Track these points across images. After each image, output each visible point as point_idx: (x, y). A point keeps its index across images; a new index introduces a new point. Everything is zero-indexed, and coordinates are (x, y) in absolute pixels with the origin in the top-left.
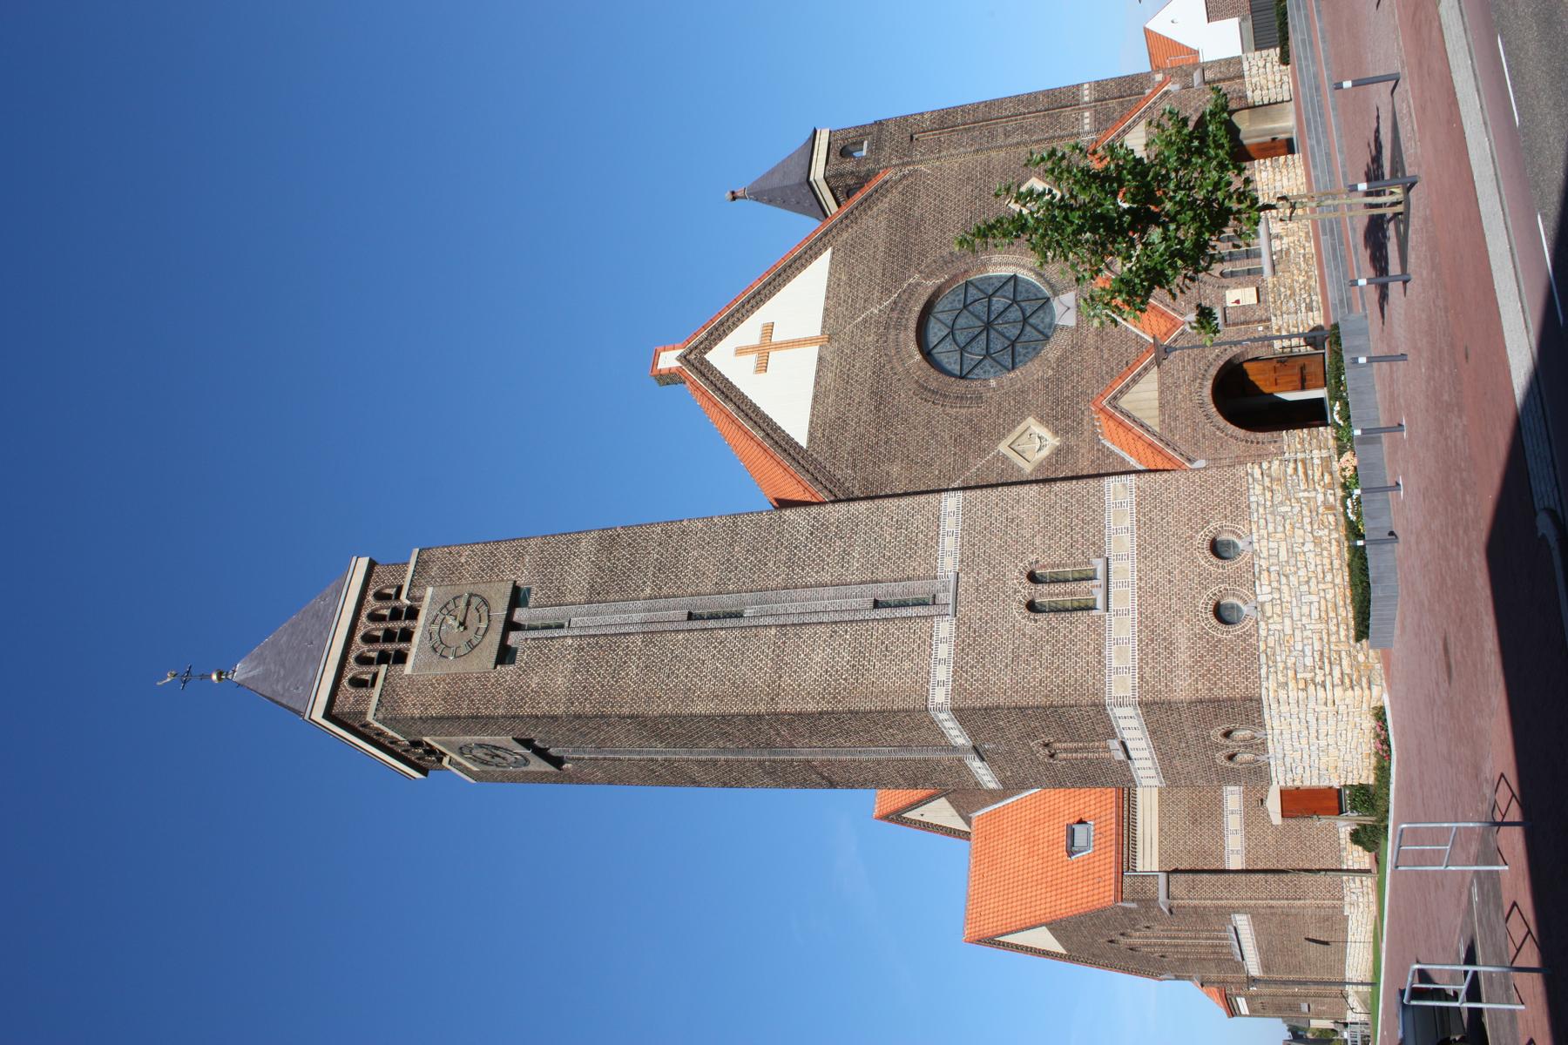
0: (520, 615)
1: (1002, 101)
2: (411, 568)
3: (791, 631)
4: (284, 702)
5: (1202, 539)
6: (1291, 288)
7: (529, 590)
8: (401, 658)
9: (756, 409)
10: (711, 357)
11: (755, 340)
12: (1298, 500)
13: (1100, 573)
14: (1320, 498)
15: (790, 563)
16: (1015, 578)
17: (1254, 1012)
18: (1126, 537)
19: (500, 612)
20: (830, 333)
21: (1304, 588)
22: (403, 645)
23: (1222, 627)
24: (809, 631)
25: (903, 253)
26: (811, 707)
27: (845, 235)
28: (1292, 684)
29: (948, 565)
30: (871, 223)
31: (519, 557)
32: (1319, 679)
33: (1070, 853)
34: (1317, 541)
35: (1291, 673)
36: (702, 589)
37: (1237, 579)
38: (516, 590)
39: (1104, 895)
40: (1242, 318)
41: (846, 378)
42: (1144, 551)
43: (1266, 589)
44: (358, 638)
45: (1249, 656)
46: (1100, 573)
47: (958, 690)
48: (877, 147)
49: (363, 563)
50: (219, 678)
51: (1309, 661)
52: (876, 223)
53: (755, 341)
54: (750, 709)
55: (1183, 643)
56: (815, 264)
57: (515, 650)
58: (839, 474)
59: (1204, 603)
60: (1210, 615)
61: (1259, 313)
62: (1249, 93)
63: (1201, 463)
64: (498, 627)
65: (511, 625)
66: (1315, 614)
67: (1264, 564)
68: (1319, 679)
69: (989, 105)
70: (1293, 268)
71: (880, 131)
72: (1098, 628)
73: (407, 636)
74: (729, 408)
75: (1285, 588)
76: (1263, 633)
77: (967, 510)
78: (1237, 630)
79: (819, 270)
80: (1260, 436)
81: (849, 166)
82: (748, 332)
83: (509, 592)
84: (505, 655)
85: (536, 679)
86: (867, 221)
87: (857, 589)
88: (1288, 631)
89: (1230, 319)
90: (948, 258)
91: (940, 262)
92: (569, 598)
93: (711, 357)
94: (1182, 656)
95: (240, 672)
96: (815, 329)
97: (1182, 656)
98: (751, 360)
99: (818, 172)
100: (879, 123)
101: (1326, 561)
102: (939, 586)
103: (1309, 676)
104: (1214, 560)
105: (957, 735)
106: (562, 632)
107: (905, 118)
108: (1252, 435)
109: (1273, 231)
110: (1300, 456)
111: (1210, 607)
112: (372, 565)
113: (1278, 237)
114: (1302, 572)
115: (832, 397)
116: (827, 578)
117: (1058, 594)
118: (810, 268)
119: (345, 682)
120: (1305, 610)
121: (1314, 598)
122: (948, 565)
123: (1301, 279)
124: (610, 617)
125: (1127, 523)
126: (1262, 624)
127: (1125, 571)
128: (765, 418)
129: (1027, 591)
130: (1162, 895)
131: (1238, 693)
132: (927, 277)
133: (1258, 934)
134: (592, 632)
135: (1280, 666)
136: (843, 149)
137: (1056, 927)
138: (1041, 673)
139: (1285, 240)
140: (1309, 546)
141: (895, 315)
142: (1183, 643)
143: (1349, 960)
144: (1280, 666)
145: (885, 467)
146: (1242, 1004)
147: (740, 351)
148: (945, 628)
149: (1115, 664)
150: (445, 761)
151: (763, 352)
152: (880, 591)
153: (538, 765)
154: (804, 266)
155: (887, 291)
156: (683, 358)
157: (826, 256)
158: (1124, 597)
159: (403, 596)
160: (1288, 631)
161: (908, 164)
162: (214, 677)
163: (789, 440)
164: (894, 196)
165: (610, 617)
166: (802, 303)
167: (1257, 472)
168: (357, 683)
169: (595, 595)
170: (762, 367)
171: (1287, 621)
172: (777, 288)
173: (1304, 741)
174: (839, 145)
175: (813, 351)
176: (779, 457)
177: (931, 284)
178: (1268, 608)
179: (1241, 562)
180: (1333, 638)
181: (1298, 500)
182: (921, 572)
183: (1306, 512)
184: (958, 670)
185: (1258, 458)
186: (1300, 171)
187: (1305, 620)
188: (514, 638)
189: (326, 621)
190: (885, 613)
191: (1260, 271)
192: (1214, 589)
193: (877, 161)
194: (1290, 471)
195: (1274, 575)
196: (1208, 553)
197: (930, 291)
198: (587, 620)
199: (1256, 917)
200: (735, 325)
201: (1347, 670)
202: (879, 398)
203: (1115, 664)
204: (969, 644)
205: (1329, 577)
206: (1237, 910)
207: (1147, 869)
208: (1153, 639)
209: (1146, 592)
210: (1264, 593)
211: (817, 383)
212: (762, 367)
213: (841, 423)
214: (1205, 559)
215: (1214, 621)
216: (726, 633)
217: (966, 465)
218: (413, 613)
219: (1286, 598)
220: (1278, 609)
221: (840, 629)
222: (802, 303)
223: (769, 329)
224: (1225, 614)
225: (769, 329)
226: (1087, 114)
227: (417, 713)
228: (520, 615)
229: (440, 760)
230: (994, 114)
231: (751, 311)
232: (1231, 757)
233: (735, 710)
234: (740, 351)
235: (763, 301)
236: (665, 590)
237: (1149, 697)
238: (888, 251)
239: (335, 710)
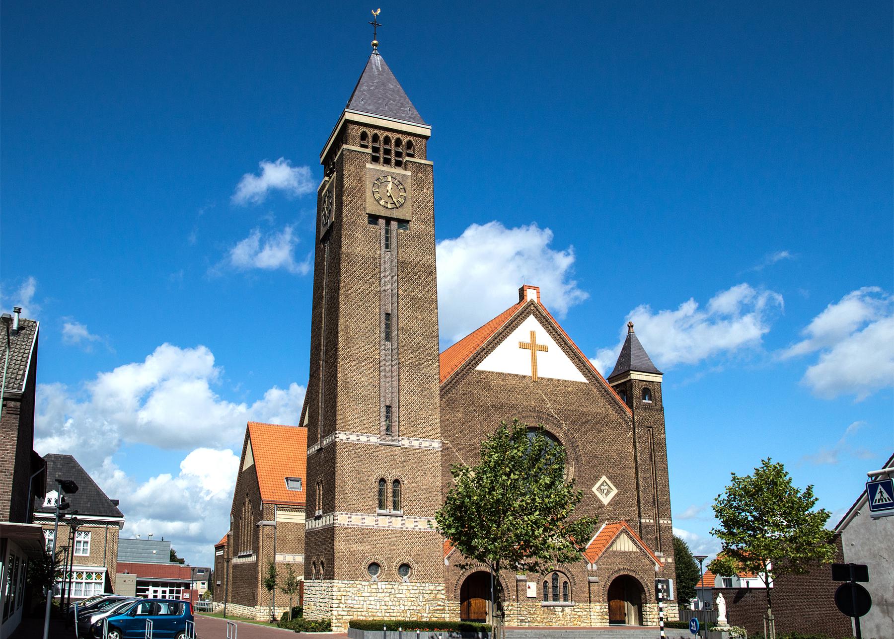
0: (394, 225)
1: (667, 477)
2: (423, 161)
3: (377, 366)
4: (356, 92)
5: (409, 560)
6: (534, 614)
7: (406, 229)
8: (375, 160)
9: (499, 343)
10: (532, 318)
11: (539, 342)
12: (425, 605)
13: (398, 513)
14: (425, 615)
15: (411, 365)
16: (395, 474)
17: (217, 558)
18: (412, 526)
19: (396, 214)
20: (539, 382)
21: (383, 603)
22: (382, 160)
23: (367, 565)
24: (376, 375)
25: (581, 421)
26: (340, 376)
27: (595, 390)
28: (339, 593)
29: (405, 442)
30: (601, 404)
31: (424, 222)
32: (341, 605)
33: (287, 479)
34: (404, 611)
35: (344, 594)
36: (401, 320)
37: (389, 574)
38: (408, 222)
39: (266, 495)
40: (520, 589)
41: (512, 390)
42: (406, 533)
43: (384, 587)
44: (387, 133)
45: (353, 576)
46: (398, 513)
47: (344, 445)
48: (647, 408)
49: (427, 132)
50: (374, 45)
51: (349, 602)
52: (601, 407)
53: (539, 342)
54: (340, 346)
55: (361, 548)
56: (580, 374)
57: (376, 224)
58: (460, 386)
59: (379, 559)
60: (373, 561)
61: (521, 597)
62: (648, 605)
63: (447, 563)
64: (388, 214)
65: (388, 220)
66: (371, 607)
67: (396, 587)
68: (341, 605)
69: (665, 470)
70: (545, 616)
71: (657, 410)
72: (370, 511)
73: (387, 162)
74: (500, 329)
75: (383, 595)
76: (363, 583)
77: (430, 451)
78: (366, 572)
79: (576, 376)
80: (459, 591)
81: (637, 393)
82: (544, 337)
83: (406, 218)
84: (373, 219)
85: (360, 236)
86: (602, 402)
87: (396, 398)
88: (364, 594)
89: (520, 584)
90: (575, 444)
91: (573, 440)
92: (400, 251)
93: (532, 318)
94: (354, 547)
95: (377, 59)
96: (541, 374)
97: (354, 547)
98: (528, 340)
99: (635, 376)
100: (662, 409)
101: (395, 614)
102: (395, 437)
103: (343, 601)
104: (399, 565)
105: (326, 442)
106: (383, 248)
107: (663, 424)
108: (459, 587)
109: (566, 609)
110: (447, 608)
111: (377, 561)
112: (426, 138)
113: (563, 611)
114: (391, 603)
115: (502, 383)
116: (402, 383)
117: (389, 495)
118: (578, 371)
119: (364, 129)
120: (373, 603)
121: (378, 607)
122: (405, 442)
123: (538, 619)
124: (387, 274)
125: (419, 527)
126: (367, 583)
127: (397, 523)
128: (493, 348)
129: (390, 479)
130: (265, 522)
131: (336, 570)
132: (565, 433)
133: (249, 565)
134: (382, 264)
135: (348, 589)
136: (648, 391)
137: (253, 467)
138: (350, 484)
139: (561, 614)
140: (403, 607)
141: (545, 416)
142: (361, 548)
143: (238, 606)
144: (348, 589)
145: (462, 410)
146: (220, 553)
147: (533, 334)
148: (374, 440)
149: (353, 517)
150: (327, 178)
151: (532, 347)
152: (395, 409)
153: (323, 232)
154: (579, 368)
155: (559, 412)
156: (532, 303)
157: (584, 380)
158: (383, 522)
159: (408, 158)
160: (364, 594)
161: (634, 425)
162: (375, 42)
163: (480, 360)
164: (615, 416)
165: (387, 274)
166: (558, 366)
167: (440, 588)
168: (364, 136)
169: (401, 265)
170: (522, 346)
171: (368, 594)
172: (567, 353)
173: (318, 596)
174: (651, 387)
175: (528, 372)
176: (471, 356)
177: (561, 436)
178: (375, 586)
179: (397, 576)
180: (359, 613)
181: (425, 605)
182: (402, 429)
183: (419, 608)
184: (354, 445)
185: (447, 589)
186: (598, 625)
187: (368, 602)
188: (382, 222)
189: (396, 115)
190: (383, 411)
191: (546, 599)
192: (385, 563)
193: (638, 408)
194: (439, 603)
195: (389, 591)
196: (402, 562)
197: (557, 435)
198: (388, 261)
199: (256, 564)
200: (548, 331)
201: (345, 618)
202: (499, 407)
203: (353, 517)
204: (367, 451)
205: (387, 614)
206: (257, 557)
207: (277, 516)
208: (363, 534)
209: (386, 533)
210: (382, 585)
211: (510, 375)
212: (522, 346)
213: (487, 387)
214: (400, 560)
215: (370, 562)
216: (380, 332)
217: (459, 450)
218: (398, 164)
219: (379, 595)
220: (374, 591)
221: (376, 390)
222: (558, 366)
223: (544, 349)
224: (374, 567)
225: (544, 349)
226: (652, 521)
227: (346, 172)
228: (394, 225)
229: (328, 175)
230: (659, 472)
231: (555, 339)
232: (314, 563)
233: (340, 338)
234: (533, 334)
235: (560, 345)
236: (401, 301)
237: (336, 531)
238: (582, 413)
239: (349, 125)
